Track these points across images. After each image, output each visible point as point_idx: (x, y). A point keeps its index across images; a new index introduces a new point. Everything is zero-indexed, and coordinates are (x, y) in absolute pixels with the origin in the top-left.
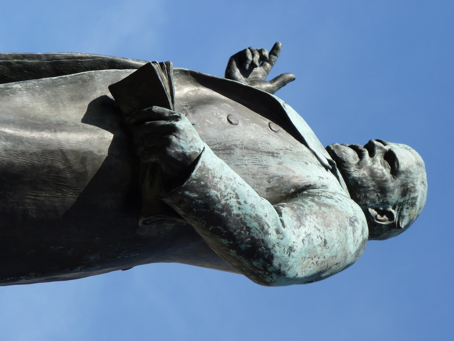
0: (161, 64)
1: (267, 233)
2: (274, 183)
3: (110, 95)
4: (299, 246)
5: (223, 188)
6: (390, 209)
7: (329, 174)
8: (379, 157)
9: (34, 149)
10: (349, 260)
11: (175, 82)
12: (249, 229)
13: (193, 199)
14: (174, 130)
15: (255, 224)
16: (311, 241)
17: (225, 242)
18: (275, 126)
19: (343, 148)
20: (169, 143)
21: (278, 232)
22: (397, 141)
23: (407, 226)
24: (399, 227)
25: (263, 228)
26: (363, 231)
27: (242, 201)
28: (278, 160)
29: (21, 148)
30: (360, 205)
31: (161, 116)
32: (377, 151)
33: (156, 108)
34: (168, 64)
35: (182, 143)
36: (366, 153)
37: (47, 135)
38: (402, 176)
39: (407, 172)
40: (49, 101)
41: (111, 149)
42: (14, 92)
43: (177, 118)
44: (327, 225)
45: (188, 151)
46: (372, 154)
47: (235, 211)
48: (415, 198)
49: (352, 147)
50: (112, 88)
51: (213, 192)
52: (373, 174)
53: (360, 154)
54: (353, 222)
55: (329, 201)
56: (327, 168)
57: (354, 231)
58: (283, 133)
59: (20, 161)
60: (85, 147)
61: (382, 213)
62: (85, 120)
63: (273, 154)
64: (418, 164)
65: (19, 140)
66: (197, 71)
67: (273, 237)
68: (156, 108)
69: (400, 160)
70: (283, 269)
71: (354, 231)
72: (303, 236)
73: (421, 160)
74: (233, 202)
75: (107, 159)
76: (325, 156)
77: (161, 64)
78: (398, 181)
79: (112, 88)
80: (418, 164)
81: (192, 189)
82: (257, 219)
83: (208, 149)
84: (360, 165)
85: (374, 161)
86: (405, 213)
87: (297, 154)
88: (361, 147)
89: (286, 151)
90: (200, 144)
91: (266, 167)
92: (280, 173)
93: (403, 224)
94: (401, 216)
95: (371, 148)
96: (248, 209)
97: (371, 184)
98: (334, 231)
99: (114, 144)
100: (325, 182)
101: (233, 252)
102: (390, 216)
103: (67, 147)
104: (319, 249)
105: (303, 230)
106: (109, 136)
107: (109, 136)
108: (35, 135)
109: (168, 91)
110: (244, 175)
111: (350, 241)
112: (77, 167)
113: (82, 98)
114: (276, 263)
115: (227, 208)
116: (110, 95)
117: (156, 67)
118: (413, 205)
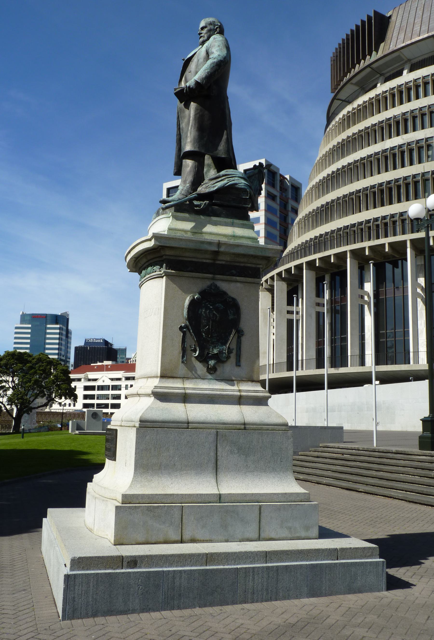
0: (175, 90)
1: (214, 62)
2: (205, 60)
3: (183, 103)
4: (218, 53)
5: (203, 74)
6: (215, 28)
7: (204, 45)
8: (202, 32)
9: (194, 122)
10: (224, 39)
11: (181, 86)
12: (213, 67)
13: (205, 81)
14: (189, 87)
15: (212, 65)
16: (218, 50)
17: (216, 73)
18: (192, 60)
19: (200, 42)
20: (192, 88)
21: (214, 59)
22: (199, 26)
23: (220, 23)
24: (220, 25)
25: (213, 63)
26: (217, 36)
27: (206, 69)
28: (200, 59)
29: (193, 125)
30: (211, 37)
31: (186, 90)
32: (201, 32)
33: (185, 91)
34: (175, 89)
35: (192, 85)
36: (201, 35)
37: (191, 119)
38: (207, 25)
39: (206, 24)
40: (184, 118)
41: (195, 102)
42: (182, 127)
43: (187, 86)
44: (214, 46)
45: (194, 83)
46: (201, 34)
47: (209, 70)
48: (213, 21)
49: (200, 38)
50: (181, 102)
51: (204, 76)
52: (206, 33)
53: (201, 37)
54: (214, 39)
55: (209, 45)
56: (203, 46)
57: (217, 38)
58: (193, 58)
59: (197, 125)
60: (194, 109)
61: (216, 30)
62: (188, 109)
63: (198, 61)
64: (204, 21)
65: (192, 125)
66: (179, 81)
67: (215, 60)
68: (185, 91)
69: (203, 26)
70: (224, 57)
71: (217, 38)
72: (216, 52)
73: (203, 20)
74: (206, 71)
75: (197, 103)
76: (201, 46)
77: (175, 90)
78: (208, 26)
79: (181, 102)
80: (204, 21)
81: (203, 82)
82: (211, 64)
83: (194, 78)
84: (204, 37)
85: (203, 33)
86: (216, 24)
87: (199, 54)
88: (200, 36)
89: (198, 57)
90: (193, 79)
91: (201, 63)
92: (203, 59)
93: (219, 24)
94: (217, 25)
95: (200, 34)
96: (209, 67)
97: (208, 34)
98: (216, 44)
99: (193, 102)
100: (206, 46)
101: (219, 71)
102: (217, 28)
103: (194, 114)
104: (220, 48)
105: (215, 52)
106: (192, 103)
107: (192, 103)
108: (191, 122)
109: (181, 89)
110: (202, 67)
111: (219, 39)
112: (199, 111)
113: (184, 110)
114: (222, 59)
115: (208, 73)
116: (183, 103)
117: (175, 92)
118: (214, 22)
